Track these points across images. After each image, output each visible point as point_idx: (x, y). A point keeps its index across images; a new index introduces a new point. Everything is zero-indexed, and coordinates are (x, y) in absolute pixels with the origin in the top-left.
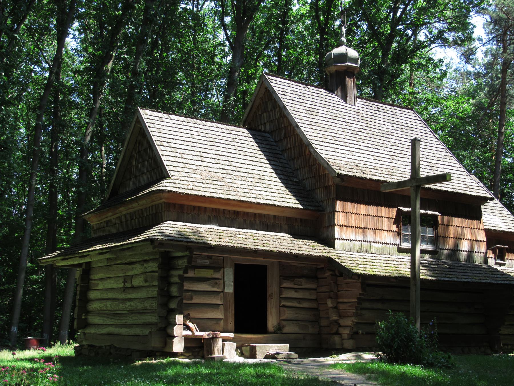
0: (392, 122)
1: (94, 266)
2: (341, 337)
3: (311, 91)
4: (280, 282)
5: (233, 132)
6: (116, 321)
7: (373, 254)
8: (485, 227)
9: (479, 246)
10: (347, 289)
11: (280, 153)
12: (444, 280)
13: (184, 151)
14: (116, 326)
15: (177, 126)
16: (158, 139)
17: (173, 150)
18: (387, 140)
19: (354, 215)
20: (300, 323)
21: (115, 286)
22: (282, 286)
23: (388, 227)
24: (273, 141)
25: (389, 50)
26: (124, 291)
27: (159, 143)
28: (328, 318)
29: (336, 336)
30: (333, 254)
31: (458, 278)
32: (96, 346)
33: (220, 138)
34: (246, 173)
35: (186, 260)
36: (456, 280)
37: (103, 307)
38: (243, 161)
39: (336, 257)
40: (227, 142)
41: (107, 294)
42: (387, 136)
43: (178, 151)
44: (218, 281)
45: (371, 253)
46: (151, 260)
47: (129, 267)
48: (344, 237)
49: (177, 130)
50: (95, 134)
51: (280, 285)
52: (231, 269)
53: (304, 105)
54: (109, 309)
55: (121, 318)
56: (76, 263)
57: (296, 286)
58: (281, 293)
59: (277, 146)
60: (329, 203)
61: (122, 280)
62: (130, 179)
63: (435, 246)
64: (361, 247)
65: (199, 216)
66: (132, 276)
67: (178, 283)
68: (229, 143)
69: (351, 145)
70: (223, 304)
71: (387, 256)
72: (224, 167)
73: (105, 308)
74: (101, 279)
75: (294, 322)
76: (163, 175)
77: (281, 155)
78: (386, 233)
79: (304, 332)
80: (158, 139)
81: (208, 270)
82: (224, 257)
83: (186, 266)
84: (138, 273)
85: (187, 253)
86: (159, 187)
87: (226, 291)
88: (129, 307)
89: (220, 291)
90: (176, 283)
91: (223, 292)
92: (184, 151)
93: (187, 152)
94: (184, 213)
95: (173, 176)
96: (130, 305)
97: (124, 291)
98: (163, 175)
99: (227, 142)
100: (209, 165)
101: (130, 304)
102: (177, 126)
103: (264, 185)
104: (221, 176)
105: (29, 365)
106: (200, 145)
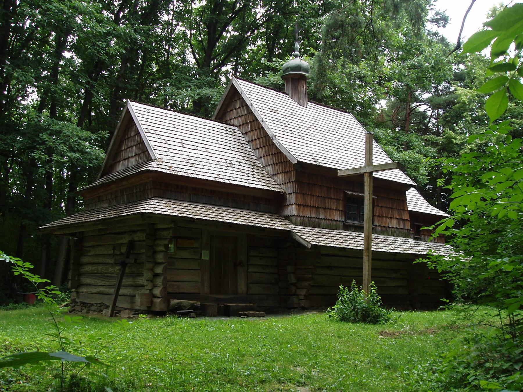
6: (107, 283)
13: (168, 138)
14: (106, 286)
16: (146, 127)
17: (159, 137)
19: (309, 197)
23: (336, 207)
27: (146, 130)
32: (88, 304)
33: (198, 128)
35: (171, 232)
38: (217, 149)
40: (203, 132)
43: (162, 137)
46: (138, 230)
47: (119, 236)
48: (301, 215)
50: (438, 91)
53: (267, 104)
54: (100, 272)
56: (71, 232)
62: (120, 161)
67: (164, 251)
68: (205, 133)
69: (306, 139)
70: (200, 270)
72: (201, 153)
73: (96, 271)
74: (93, 247)
76: (149, 159)
80: (146, 127)
83: (171, 236)
85: (172, 225)
87: (203, 258)
89: (197, 258)
90: (162, 251)
91: (200, 259)
92: (168, 138)
93: (171, 139)
98: (149, 159)
99: (203, 132)
100: (190, 150)
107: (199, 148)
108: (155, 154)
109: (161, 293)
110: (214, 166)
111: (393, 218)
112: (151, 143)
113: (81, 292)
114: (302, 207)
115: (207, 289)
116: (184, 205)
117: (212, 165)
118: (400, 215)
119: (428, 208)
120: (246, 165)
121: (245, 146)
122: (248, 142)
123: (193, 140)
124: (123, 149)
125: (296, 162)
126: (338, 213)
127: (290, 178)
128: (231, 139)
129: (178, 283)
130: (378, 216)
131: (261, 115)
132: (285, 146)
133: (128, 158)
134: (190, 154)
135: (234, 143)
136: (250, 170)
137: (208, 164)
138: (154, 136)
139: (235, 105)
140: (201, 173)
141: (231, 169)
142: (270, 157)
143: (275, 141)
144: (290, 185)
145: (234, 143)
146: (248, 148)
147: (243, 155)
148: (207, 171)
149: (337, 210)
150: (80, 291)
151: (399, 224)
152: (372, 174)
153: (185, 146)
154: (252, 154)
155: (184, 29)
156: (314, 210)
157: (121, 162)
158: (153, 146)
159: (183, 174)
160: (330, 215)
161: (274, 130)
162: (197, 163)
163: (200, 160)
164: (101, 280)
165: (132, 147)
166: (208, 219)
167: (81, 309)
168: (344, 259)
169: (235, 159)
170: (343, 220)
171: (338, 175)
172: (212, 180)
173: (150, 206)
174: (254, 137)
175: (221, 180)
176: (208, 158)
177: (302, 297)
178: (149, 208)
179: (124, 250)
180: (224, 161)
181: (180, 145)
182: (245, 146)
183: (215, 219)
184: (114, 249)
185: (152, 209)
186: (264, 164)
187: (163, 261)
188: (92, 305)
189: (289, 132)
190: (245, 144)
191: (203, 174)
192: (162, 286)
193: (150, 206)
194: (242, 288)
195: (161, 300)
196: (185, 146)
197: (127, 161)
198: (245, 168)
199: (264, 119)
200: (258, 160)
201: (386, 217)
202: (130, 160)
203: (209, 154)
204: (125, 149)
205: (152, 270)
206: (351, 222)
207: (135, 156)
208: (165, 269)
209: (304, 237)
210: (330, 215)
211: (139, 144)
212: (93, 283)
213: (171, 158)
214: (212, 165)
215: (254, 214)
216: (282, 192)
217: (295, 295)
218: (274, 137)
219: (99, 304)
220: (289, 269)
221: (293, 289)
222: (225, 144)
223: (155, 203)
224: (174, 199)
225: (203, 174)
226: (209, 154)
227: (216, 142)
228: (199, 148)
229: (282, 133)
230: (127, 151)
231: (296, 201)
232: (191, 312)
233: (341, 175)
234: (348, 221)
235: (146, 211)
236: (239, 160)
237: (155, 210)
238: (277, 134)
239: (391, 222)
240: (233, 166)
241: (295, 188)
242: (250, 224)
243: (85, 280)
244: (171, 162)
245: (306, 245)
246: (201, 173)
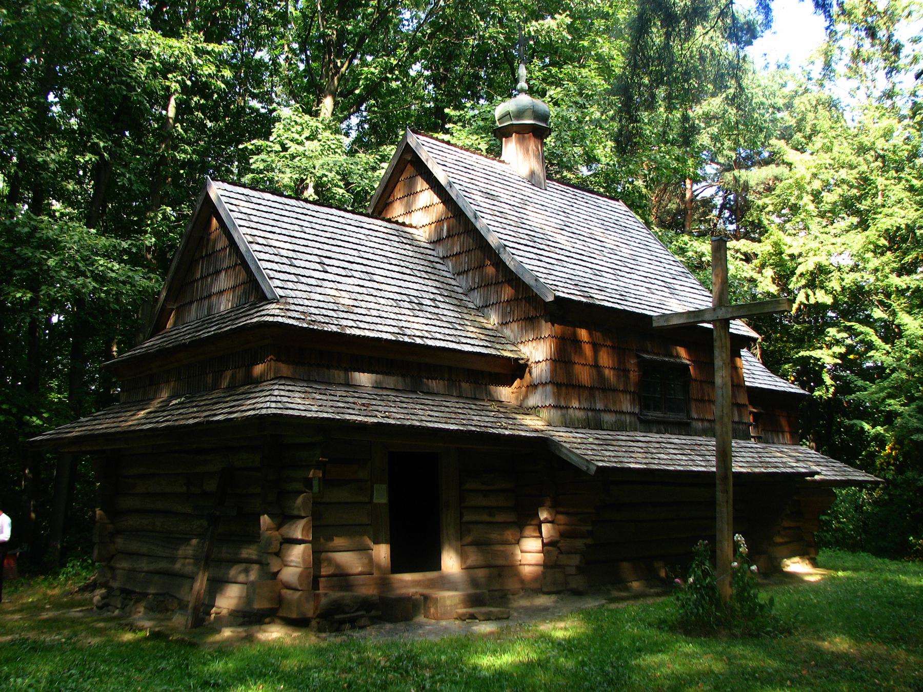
15: (275, 211)
16: (249, 231)
25: (858, 418)
27: (250, 239)
34: (361, 272)
49: (277, 217)
62: (191, 303)
64: (587, 420)
68: (362, 242)
70: (371, 525)
78: (621, 395)
80: (249, 231)
86: (261, 316)
87: (375, 500)
91: (371, 502)
93: (300, 256)
100: (338, 279)
102: (275, 211)
105: (661, 664)
106: (318, 245)
107: (355, 274)
108: (275, 285)
110: (389, 309)
112: (263, 265)
113: (119, 569)
114: (564, 389)
116: (339, 393)
117: (385, 308)
119: (770, 379)
120: (447, 307)
121: (438, 266)
122: (443, 258)
123: (342, 257)
125: (550, 298)
126: (628, 397)
128: (411, 254)
130: (696, 400)
131: (472, 205)
132: (527, 267)
134: (340, 286)
135: (417, 261)
136: (457, 315)
137: (377, 307)
138: (267, 249)
140: (366, 326)
141: (420, 314)
143: (504, 257)
145: (417, 261)
146: (446, 269)
147: (438, 285)
148: (378, 320)
149: (625, 392)
150: (118, 566)
152: (729, 323)
153: (329, 269)
154: (454, 283)
156: (586, 393)
157: (195, 305)
158: (268, 271)
159: (335, 329)
160: (615, 403)
161: (500, 235)
162: (356, 303)
163: (359, 297)
166: (392, 422)
169: (425, 294)
170: (637, 410)
171: (654, 325)
172: (391, 340)
173: (274, 399)
174: (457, 249)
175: (406, 339)
176: (375, 293)
177: (573, 571)
178: (273, 405)
179: (211, 486)
180: (405, 298)
181: (319, 267)
182: (438, 266)
183: (408, 423)
185: (279, 405)
186: (479, 302)
189: (527, 237)
190: (437, 263)
191: (372, 327)
193: (274, 399)
195: (301, 596)
196: (329, 269)
197: (206, 302)
198: (446, 312)
199: (478, 213)
200: (466, 295)
203: (376, 285)
204: (202, 278)
206: (653, 415)
209: (578, 452)
210: (615, 403)
213: (305, 295)
214: (385, 308)
215: (473, 407)
218: (502, 250)
222: (402, 264)
223: (282, 393)
224: (316, 382)
225: (372, 327)
226: (376, 285)
227: (385, 260)
228: (355, 274)
229: (515, 240)
230: (207, 281)
232: (362, 616)
233: (660, 325)
234: (645, 412)
235: (269, 411)
236: (432, 296)
237: (287, 409)
238: (506, 243)
240: (424, 308)
242: (474, 429)
244: (307, 303)
246: (366, 326)
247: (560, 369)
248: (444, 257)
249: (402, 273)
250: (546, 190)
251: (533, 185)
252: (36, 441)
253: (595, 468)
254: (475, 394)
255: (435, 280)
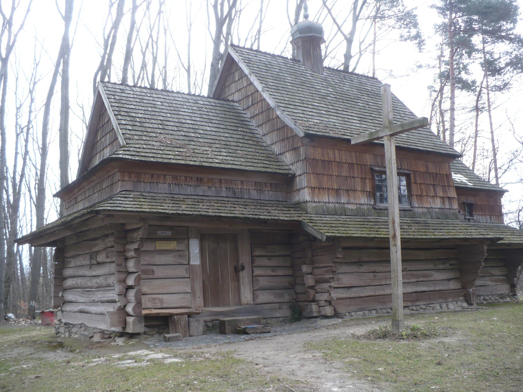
0: (359, 89)
1: (68, 244)
2: (318, 304)
3: (278, 61)
4: (251, 251)
5: (199, 102)
7: (348, 216)
8: (455, 185)
9: (451, 203)
10: (322, 254)
11: (249, 120)
12: (422, 239)
18: (356, 104)
20: (275, 291)
21: (84, 263)
22: (254, 274)
24: (241, 109)
26: (90, 268)
28: (304, 284)
29: (313, 303)
30: (305, 218)
31: (435, 235)
36: (433, 237)
37: (75, 284)
39: (308, 221)
41: (78, 272)
42: (355, 101)
44: (182, 252)
45: (346, 215)
47: (94, 243)
48: (316, 200)
51: (252, 254)
52: (197, 239)
55: (90, 296)
57: (269, 254)
58: (253, 262)
59: (245, 114)
60: (299, 166)
61: (88, 257)
62: (97, 154)
63: (409, 205)
65: (157, 185)
66: (97, 252)
71: (363, 217)
73: (76, 286)
75: (268, 291)
77: (250, 122)
79: (279, 300)
81: (171, 242)
82: (187, 227)
84: (102, 249)
88: (96, 285)
91: (188, 264)
94: (141, 181)
95: (127, 144)
96: (96, 283)
97: (90, 268)
101: (97, 281)
103: (230, 151)
104: (183, 142)
109: (134, 309)
111: (436, 196)
115: (200, 301)
118: (445, 191)
124: (99, 139)
127: (300, 155)
129: (160, 296)
133: (103, 149)
139: (234, 77)
142: (275, 133)
144: (299, 164)
151: (443, 203)
155: (262, 93)
164: (81, 296)
165: (106, 135)
167: (65, 331)
168: (420, 258)
174: (257, 112)
184: (91, 258)
187: (135, 271)
188: (74, 325)
192: (134, 301)
194: (247, 296)
195: (135, 320)
201: (427, 196)
202: (105, 150)
204: (100, 139)
205: (124, 281)
207: (109, 145)
208: (138, 280)
210: (355, 199)
211: (112, 130)
212: (74, 299)
216: (291, 174)
217: (313, 301)
219: (80, 324)
220: (305, 269)
221: (312, 292)
227: (208, 121)
231: (308, 183)
239: (434, 202)
241: (305, 168)
243: (69, 296)
245: (320, 238)
247: (314, 178)
248: (250, 118)
249: (218, 128)
250: (323, 74)
251: (313, 72)
252: (229, 293)
253: (325, 237)
254: (260, 197)
255: (216, 127)
